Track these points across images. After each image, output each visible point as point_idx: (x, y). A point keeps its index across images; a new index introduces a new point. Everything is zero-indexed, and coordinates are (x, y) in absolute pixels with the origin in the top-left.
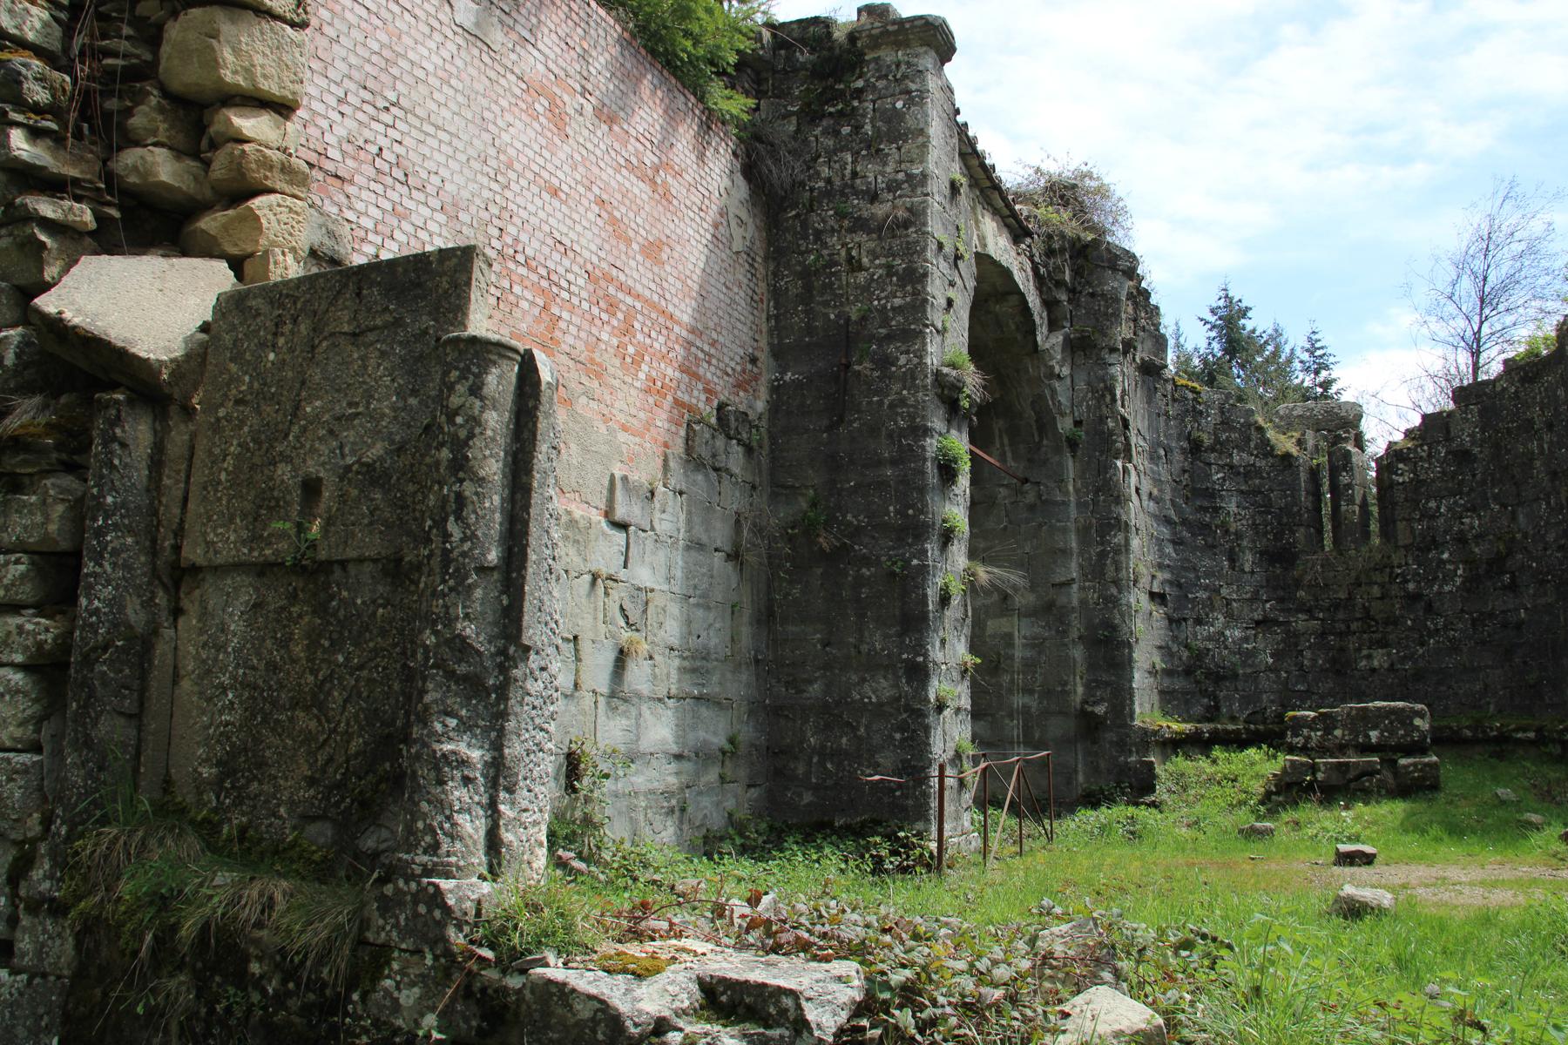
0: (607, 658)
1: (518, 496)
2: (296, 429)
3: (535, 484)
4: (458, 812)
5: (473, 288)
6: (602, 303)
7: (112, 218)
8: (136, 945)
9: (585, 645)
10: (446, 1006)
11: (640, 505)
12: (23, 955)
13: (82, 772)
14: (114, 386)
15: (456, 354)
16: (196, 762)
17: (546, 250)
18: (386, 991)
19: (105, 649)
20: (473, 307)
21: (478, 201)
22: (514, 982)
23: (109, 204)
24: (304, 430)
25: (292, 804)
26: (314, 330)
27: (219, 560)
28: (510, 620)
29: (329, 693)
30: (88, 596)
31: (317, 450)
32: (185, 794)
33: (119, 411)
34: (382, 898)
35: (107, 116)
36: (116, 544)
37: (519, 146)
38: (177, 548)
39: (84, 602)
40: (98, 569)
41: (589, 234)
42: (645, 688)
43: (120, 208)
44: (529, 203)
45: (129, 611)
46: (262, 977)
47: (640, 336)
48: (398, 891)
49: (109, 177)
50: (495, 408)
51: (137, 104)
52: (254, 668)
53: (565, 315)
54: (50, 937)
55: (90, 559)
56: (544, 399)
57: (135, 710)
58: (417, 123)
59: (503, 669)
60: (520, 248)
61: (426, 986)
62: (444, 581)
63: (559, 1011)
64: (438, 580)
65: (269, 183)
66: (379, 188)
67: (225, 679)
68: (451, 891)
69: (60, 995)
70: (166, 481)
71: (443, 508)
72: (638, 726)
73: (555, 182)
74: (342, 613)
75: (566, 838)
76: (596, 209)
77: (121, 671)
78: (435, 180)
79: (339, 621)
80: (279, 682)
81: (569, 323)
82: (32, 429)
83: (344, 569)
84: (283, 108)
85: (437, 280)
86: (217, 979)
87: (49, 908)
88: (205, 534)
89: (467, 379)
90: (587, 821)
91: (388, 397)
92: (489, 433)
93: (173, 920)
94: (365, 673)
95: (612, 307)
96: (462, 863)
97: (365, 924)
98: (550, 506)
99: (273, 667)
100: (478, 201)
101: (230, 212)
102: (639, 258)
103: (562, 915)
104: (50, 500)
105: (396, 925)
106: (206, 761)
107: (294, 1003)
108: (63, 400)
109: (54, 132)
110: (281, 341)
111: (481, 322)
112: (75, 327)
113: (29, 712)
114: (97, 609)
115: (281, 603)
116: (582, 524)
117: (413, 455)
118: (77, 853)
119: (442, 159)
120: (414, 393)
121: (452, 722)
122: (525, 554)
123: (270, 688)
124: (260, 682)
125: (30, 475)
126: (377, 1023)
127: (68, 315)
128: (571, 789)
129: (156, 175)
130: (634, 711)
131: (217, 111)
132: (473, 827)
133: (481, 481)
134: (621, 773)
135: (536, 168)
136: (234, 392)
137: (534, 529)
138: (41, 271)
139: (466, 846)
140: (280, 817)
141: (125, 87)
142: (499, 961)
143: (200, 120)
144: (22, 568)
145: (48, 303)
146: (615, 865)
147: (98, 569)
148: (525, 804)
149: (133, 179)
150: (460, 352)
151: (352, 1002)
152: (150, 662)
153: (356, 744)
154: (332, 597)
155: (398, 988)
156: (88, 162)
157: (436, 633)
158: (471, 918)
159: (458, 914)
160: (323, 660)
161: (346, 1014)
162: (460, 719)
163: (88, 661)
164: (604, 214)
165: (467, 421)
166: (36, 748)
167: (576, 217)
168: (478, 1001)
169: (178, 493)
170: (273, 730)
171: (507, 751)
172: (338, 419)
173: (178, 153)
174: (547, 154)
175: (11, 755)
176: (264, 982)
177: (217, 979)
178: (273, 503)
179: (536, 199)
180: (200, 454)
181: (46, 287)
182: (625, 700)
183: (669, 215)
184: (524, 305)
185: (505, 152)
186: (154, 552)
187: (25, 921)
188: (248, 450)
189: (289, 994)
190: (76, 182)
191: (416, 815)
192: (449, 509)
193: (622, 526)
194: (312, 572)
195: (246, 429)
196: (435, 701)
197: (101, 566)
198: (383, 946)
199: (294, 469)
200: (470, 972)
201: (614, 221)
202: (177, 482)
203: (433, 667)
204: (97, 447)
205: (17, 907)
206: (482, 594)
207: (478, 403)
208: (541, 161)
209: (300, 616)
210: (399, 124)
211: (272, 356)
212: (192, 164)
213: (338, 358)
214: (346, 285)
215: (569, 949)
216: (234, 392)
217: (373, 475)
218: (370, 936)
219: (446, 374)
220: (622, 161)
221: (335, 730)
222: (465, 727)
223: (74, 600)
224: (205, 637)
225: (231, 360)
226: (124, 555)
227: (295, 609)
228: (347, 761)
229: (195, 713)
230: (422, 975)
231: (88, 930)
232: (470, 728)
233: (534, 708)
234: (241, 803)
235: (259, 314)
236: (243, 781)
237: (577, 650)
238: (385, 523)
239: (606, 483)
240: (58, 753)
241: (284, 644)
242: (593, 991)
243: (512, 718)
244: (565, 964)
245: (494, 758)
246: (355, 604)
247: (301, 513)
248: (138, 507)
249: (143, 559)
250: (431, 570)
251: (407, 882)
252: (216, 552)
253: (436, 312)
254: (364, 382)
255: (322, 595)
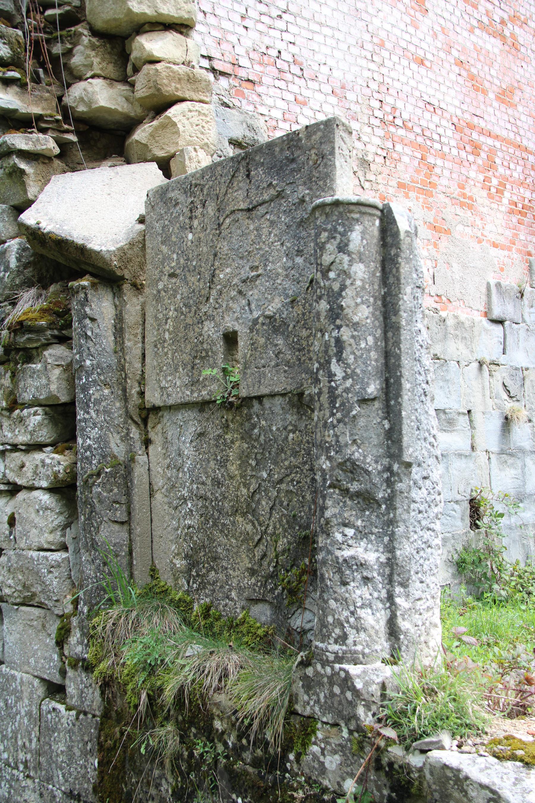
0: (497, 423)
1: (390, 334)
2: (214, 292)
3: (403, 323)
4: (361, 607)
5: (337, 155)
6: (468, 148)
7: (73, 143)
8: (136, 701)
9: (477, 416)
10: (362, 774)
11: (512, 304)
12: (72, 697)
13: (93, 567)
14: (80, 275)
15: (324, 217)
16: (170, 556)
17: (419, 112)
18: (314, 755)
19: (99, 475)
20: (338, 172)
21: (360, 81)
22: (416, 760)
23: (67, 131)
24: (220, 293)
25: (240, 590)
26: (219, 210)
27: (171, 402)
28: (393, 438)
29: (258, 502)
30: (82, 436)
31: (231, 308)
32: (166, 579)
33: (86, 294)
34: (305, 677)
35: (55, 59)
36: (97, 396)
37: (388, 27)
38: (142, 394)
39: (80, 440)
40: (87, 416)
41: (452, 92)
42: (527, 444)
43: (77, 133)
44: (401, 74)
45: (113, 445)
46: (223, 733)
47: (501, 170)
48: (317, 673)
49: (65, 110)
50: (361, 261)
51: (75, 45)
52: (203, 483)
53: (439, 162)
54: (86, 687)
55: (81, 409)
56: (404, 247)
57: (125, 519)
58: (304, 23)
59: (389, 483)
60: (397, 114)
61: (344, 755)
62: (333, 415)
63: (456, 794)
64: (328, 414)
65: (179, 94)
66: (282, 84)
67: (185, 493)
68: (358, 676)
69: (95, 728)
70: (128, 344)
71: (326, 352)
72: (524, 474)
73: (421, 53)
74: (262, 438)
75: (473, 563)
76: (456, 69)
77: (111, 491)
78: (325, 70)
79: (261, 445)
80: (222, 494)
81: (443, 167)
82: (31, 315)
83: (261, 403)
84: (182, 27)
85: (303, 155)
86: (193, 730)
87: (83, 666)
88: (159, 381)
89: (334, 238)
90: (490, 550)
91: (280, 259)
92: (359, 283)
93: (159, 683)
94: (283, 486)
95: (476, 148)
96: (367, 651)
97: (293, 699)
98: (420, 338)
99: (217, 483)
100: (360, 81)
101: (155, 123)
102: (496, 104)
103: (454, 700)
104: (49, 367)
105: (318, 701)
106: (178, 554)
107: (247, 756)
108: (52, 288)
109: (19, 80)
110: (196, 223)
111: (346, 186)
112: (49, 233)
113: (56, 522)
114: (90, 446)
115: (218, 432)
116: (467, 324)
117: (304, 306)
118: (94, 628)
119: (328, 51)
120: (299, 253)
121: (350, 532)
122: (400, 384)
123: (216, 498)
124: (209, 494)
125: (37, 348)
126: (308, 780)
127: (42, 225)
128: (474, 526)
129: (96, 103)
130: (519, 463)
131: (133, 39)
132: (375, 619)
133: (356, 326)
134: (512, 511)
135: (404, 44)
136: (167, 268)
137: (406, 362)
138: (25, 192)
139: (370, 636)
140: (232, 600)
141: (64, 33)
142: (402, 738)
143: (124, 50)
144: (39, 418)
145: (29, 217)
146: (513, 583)
147: (87, 416)
148: (418, 594)
149: (81, 108)
150: (327, 215)
151: (289, 761)
152: (131, 481)
153: (282, 544)
154: (254, 426)
155: (323, 754)
156: (46, 100)
157: (329, 458)
158: (377, 698)
159: (366, 696)
160: (252, 476)
161: (286, 770)
162: (357, 528)
163: (88, 486)
164: (464, 73)
165: (338, 275)
166: (64, 548)
167: (441, 80)
168: (387, 774)
169: (138, 352)
170: (222, 531)
171: (398, 553)
172: (244, 281)
173: (110, 80)
174: (411, 30)
175: (48, 554)
176: (225, 737)
177: (193, 730)
178: (204, 354)
179: (407, 71)
180: (149, 320)
181: (29, 203)
182: (511, 455)
183: (518, 62)
184: (406, 159)
185: (377, 36)
186: (125, 398)
187: (70, 673)
188: (182, 313)
189: (243, 748)
190: (39, 118)
191: (325, 611)
192: (331, 353)
193: (500, 322)
194: (238, 406)
195: (179, 297)
196: (335, 516)
197: (88, 413)
198: (309, 717)
199: (217, 325)
200: (378, 749)
201: (472, 77)
202: (136, 343)
203: (330, 487)
204: (75, 325)
205: (64, 663)
206: (371, 420)
207: (346, 258)
208: (407, 37)
209: (232, 442)
210: (291, 28)
211: (190, 236)
212: (122, 88)
213: (239, 231)
214: (238, 170)
215: (465, 730)
216: (167, 268)
217: (274, 325)
218: (298, 708)
219: (318, 235)
220: (475, 23)
221: (266, 532)
222: (362, 534)
223: (74, 438)
224: (168, 460)
225: (163, 243)
226: (104, 404)
227: (228, 437)
228: (277, 556)
229: (167, 518)
230: (340, 745)
231: (107, 684)
232: (366, 535)
233: (420, 512)
234: (204, 588)
235: (177, 204)
236: (204, 571)
237: (471, 421)
238: (288, 363)
239: (484, 290)
240: (77, 552)
241: (223, 463)
242: (485, 780)
243: (400, 524)
244: (459, 746)
245: (388, 559)
246: (271, 430)
247: (225, 360)
248: (109, 366)
249: (118, 404)
250: (321, 405)
251: (323, 667)
252: (169, 395)
253: (309, 181)
254: (260, 249)
255: (247, 425)
